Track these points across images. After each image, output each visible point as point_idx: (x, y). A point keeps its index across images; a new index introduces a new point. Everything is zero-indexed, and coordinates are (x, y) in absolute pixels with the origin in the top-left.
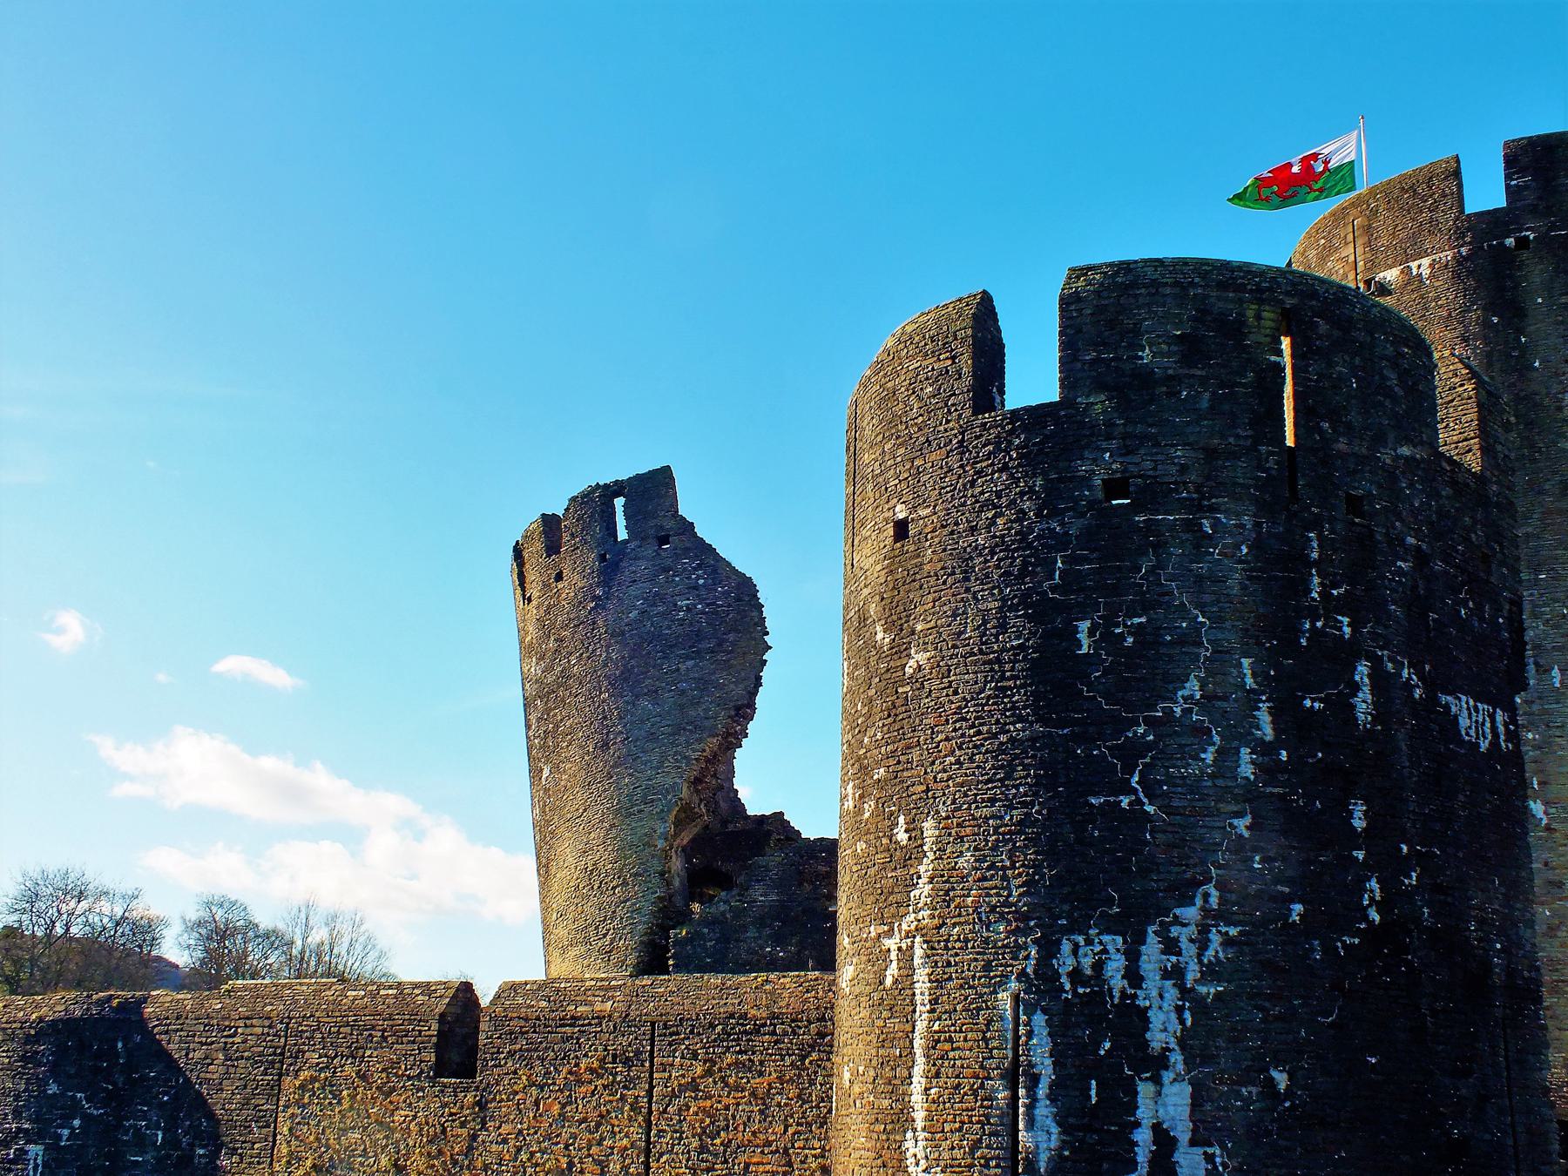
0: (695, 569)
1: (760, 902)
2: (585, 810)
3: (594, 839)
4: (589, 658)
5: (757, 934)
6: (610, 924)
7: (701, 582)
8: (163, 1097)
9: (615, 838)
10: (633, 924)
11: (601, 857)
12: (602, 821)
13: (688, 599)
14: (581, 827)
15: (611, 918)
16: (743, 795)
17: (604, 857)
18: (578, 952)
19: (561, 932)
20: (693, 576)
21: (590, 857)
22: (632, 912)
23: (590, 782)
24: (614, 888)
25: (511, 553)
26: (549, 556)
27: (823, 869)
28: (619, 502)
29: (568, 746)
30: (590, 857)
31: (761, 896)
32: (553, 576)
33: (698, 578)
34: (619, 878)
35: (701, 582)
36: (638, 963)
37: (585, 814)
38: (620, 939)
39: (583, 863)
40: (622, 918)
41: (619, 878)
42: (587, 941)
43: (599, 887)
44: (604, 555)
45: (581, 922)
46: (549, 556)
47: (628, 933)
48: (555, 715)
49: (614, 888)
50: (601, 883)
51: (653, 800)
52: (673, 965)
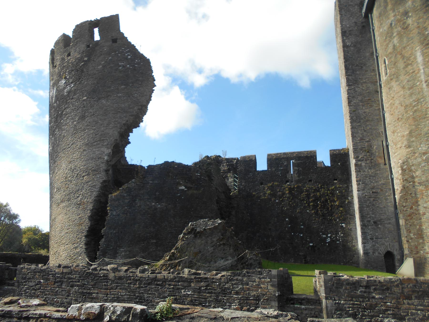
0: (127, 52)
1: (150, 183)
2: (72, 144)
3: (75, 156)
4: (79, 84)
5: (149, 197)
6: (81, 192)
7: (129, 57)
8: (302, 225)
9: (85, 156)
10: (91, 192)
11: (78, 164)
12: (79, 148)
13: (124, 63)
14: (70, 152)
15: (82, 189)
16: (126, 155)
17: (80, 164)
18: (65, 205)
19: (58, 196)
20: (126, 55)
21: (73, 164)
22: (91, 187)
23: (75, 133)
24: (83, 176)
25: (49, 53)
26: (65, 48)
27: (350, 78)
28: (96, 30)
29: (66, 119)
30: (73, 164)
31: (151, 181)
32: (66, 55)
33: (128, 55)
34: (86, 172)
35: (129, 57)
36: (93, 209)
37: (72, 146)
38: (85, 198)
39: (70, 166)
40: (86, 190)
41: (86, 172)
42: (69, 200)
43: (76, 177)
44: (89, 45)
45: (67, 192)
46: (65, 48)
47: (89, 196)
48: (62, 108)
49: (83, 176)
50: (77, 175)
51: (103, 140)
52: (110, 210)
